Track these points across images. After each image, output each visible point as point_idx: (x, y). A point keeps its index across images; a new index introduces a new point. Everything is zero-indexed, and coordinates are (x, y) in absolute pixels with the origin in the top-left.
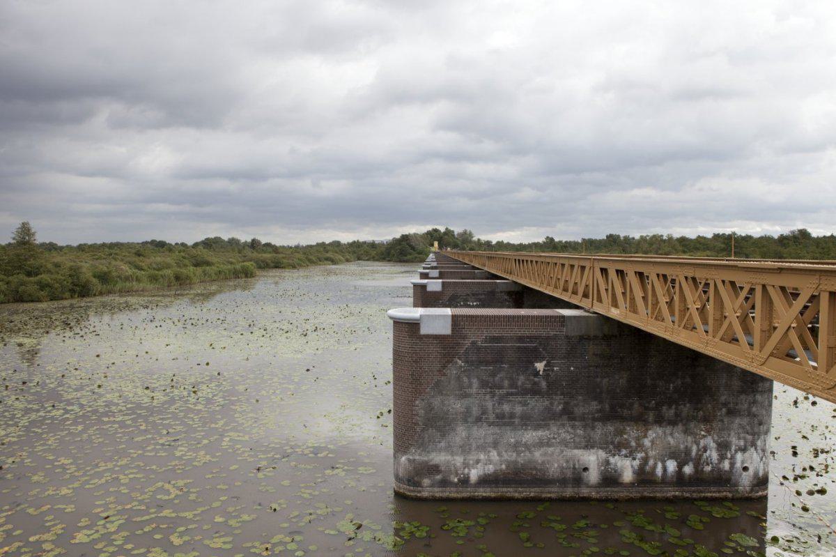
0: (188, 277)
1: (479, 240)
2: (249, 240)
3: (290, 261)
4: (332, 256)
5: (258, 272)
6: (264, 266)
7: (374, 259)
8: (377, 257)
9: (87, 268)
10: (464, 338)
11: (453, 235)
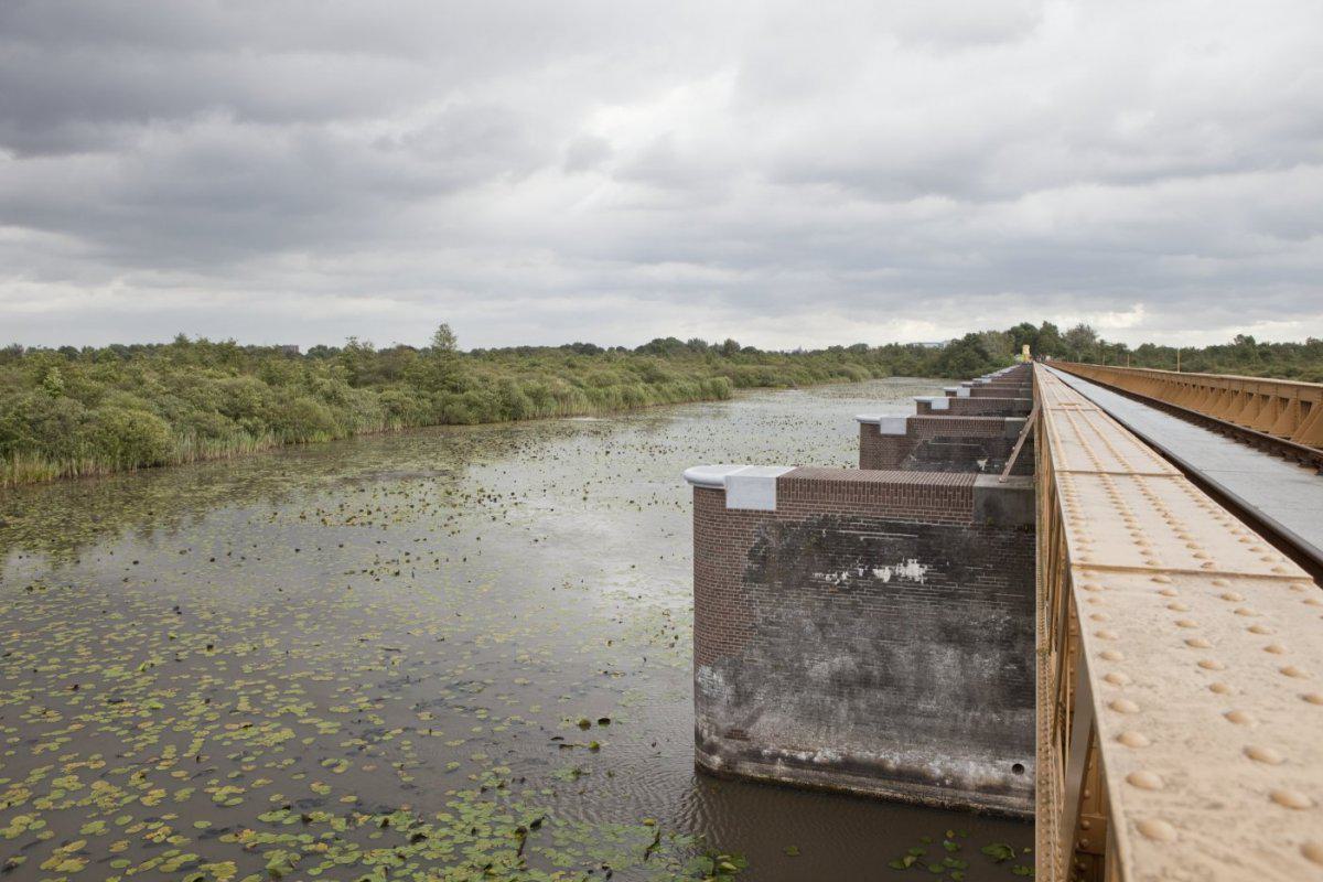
0: (640, 399)
1: (1102, 342)
2: (721, 342)
3: (786, 377)
4: (850, 369)
5: (734, 392)
6: (744, 383)
7: (921, 374)
8: (925, 371)
9: (520, 385)
10: (917, 437)
11: (1056, 334)
